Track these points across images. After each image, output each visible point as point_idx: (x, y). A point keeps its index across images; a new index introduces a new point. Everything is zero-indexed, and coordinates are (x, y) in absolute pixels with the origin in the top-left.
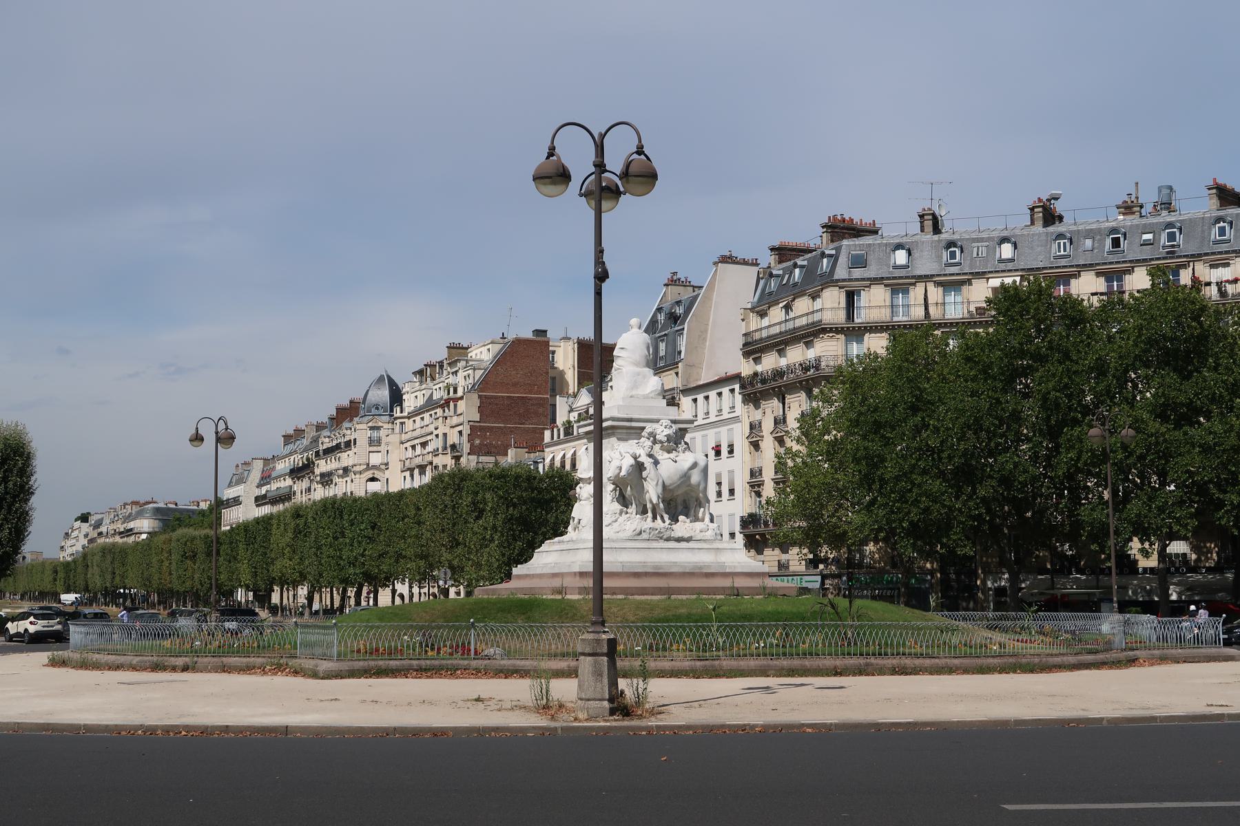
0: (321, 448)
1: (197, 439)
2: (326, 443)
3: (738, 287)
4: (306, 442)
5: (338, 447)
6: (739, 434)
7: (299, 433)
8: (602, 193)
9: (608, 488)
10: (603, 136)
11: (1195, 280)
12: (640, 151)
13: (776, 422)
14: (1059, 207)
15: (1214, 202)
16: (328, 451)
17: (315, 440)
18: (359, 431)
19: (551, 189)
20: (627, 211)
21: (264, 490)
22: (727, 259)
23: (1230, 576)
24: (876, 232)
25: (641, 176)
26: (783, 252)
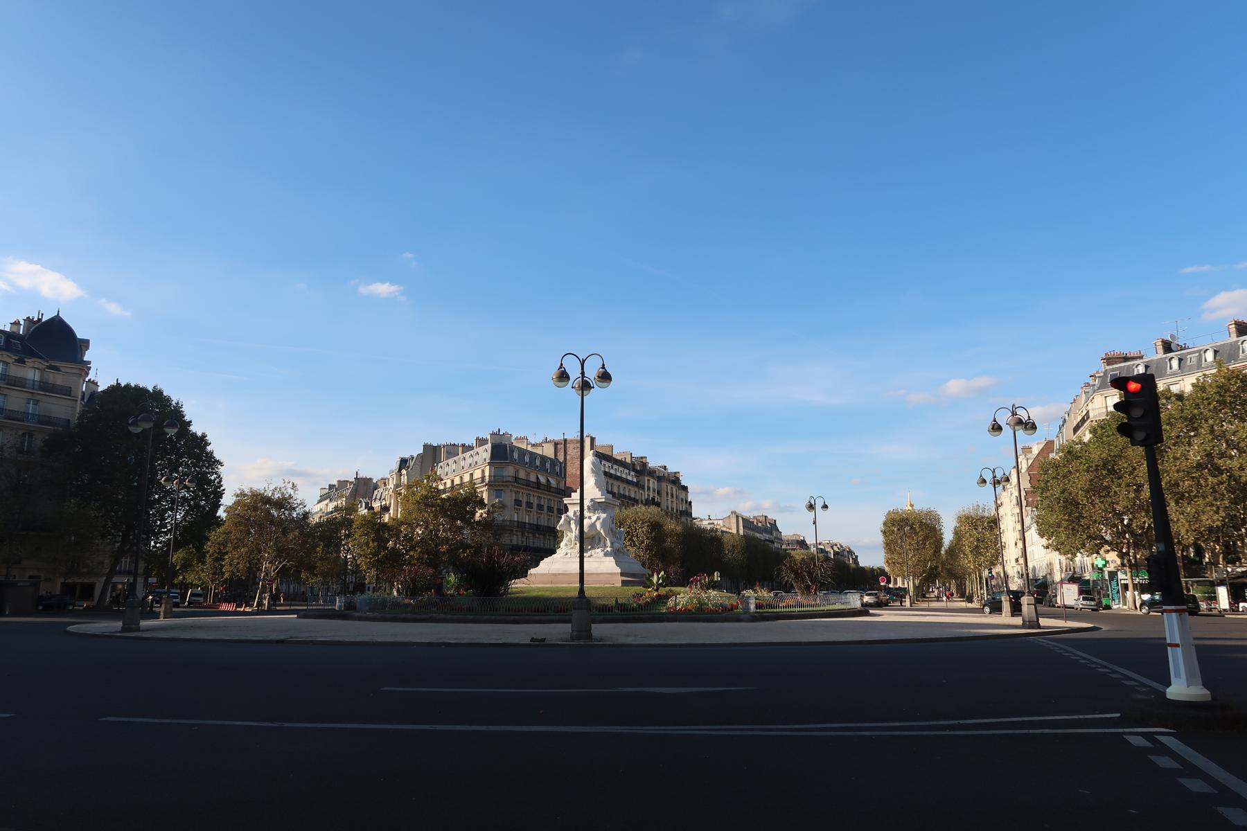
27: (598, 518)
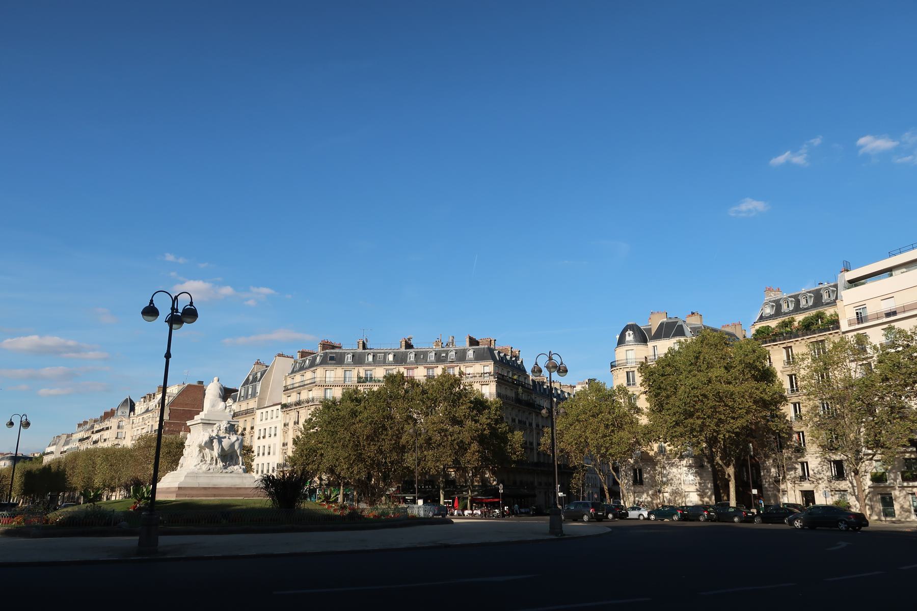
0: (95, 430)
1: (11, 424)
2: (97, 427)
3: (286, 365)
4: (88, 426)
5: (103, 430)
6: (280, 427)
7: (86, 423)
8: (175, 320)
9: (163, 450)
10: (176, 297)
11: (461, 373)
12: (191, 304)
13: (295, 423)
14: (412, 342)
15: (468, 343)
16: (98, 432)
17: (92, 427)
18: (113, 422)
19: (150, 318)
20: (183, 332)
21: (66, 448)
22: (279, 355)
23: (685, 485)
24: (340, 348)
25: (191, 314)
26: (304, 354)
27: (238, 439)
